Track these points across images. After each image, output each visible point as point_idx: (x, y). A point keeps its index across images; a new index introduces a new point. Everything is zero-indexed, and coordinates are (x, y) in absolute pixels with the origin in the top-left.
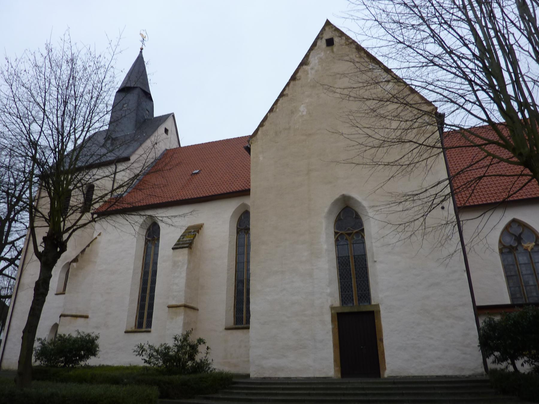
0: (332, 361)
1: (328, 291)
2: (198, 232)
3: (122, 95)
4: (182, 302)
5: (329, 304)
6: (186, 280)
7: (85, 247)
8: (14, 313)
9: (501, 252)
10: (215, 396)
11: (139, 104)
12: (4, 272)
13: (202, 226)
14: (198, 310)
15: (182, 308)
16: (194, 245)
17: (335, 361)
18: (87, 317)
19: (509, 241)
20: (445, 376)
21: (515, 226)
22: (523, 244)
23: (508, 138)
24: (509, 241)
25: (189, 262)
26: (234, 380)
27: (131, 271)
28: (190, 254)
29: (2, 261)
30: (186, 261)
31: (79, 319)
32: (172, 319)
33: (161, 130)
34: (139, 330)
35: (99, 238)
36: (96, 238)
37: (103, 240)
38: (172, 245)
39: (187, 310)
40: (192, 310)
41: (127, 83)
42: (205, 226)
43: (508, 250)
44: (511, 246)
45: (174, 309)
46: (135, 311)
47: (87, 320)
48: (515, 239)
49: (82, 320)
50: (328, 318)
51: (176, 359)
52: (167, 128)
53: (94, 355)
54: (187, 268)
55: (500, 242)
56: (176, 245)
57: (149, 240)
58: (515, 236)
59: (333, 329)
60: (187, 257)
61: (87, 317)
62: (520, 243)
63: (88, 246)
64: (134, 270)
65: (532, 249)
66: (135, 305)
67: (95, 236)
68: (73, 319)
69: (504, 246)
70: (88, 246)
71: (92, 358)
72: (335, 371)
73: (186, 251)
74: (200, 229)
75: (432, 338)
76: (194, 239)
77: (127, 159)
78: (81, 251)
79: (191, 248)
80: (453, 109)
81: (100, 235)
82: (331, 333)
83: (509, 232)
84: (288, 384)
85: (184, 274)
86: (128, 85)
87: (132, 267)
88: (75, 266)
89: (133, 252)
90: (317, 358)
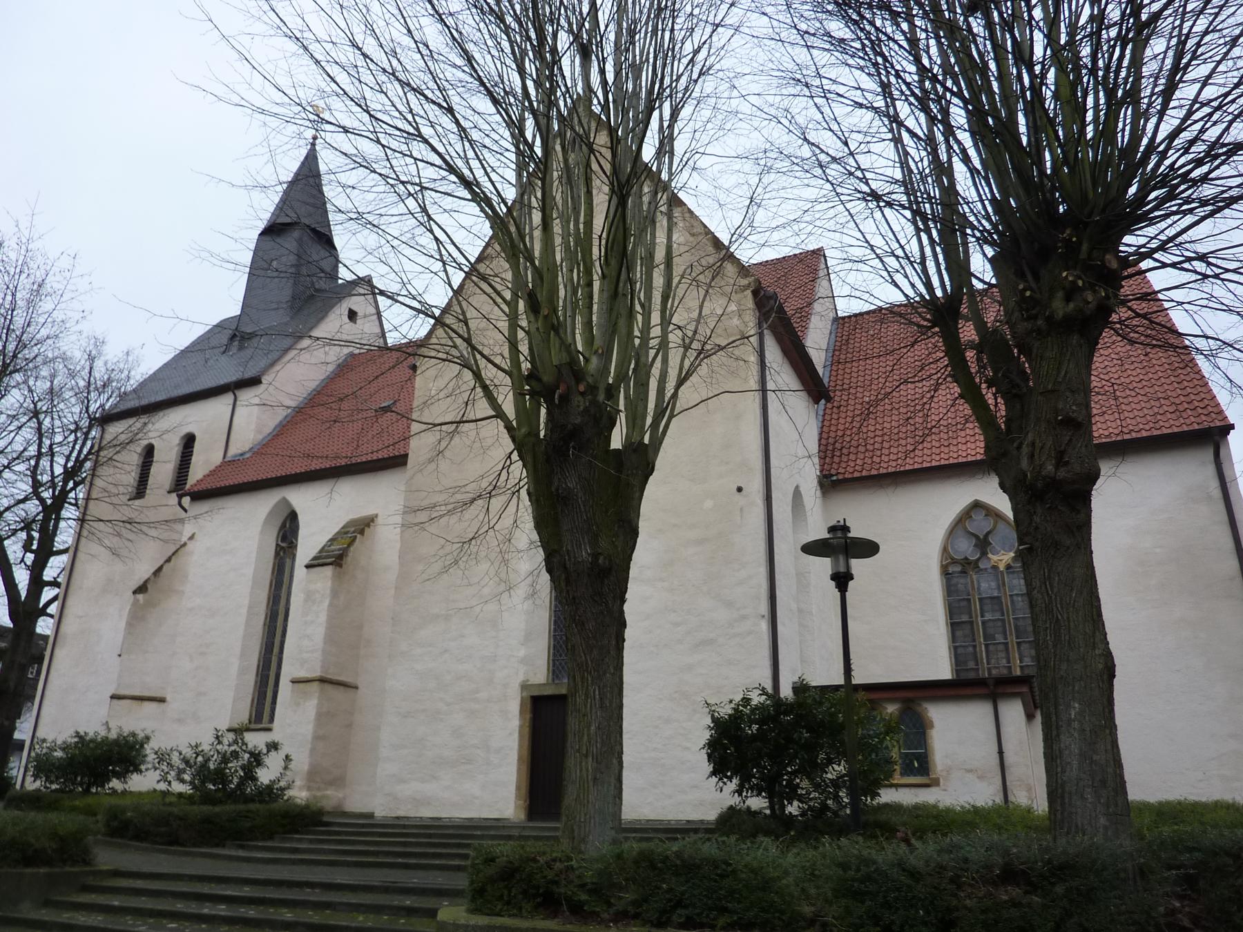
0: (513, 788)
1: (522, 653)
2: (362, 532)
3: (269, 243)
4: (317, 673)
5: (521, 678)
6: (327, 628)
7: (161, 562)
8: (47, 693)
9: (945, 572)
10: (269, 844)
11: (301, 259)
12: (49, 611)
13: (373, 521)
14: (357, 688)
15: (316, 685)
16: (349, 559)
17: (518, 788)
18: (162, 700)
19: (965, 548)
20: (702, 822)
21: (978, 516)
22: (990, 555)
23: (1071, 305)
24: (965, 548)
25: (335, 594)
26: (325, 819)
27: (244, 611)
28: (337, 578)
29: (46, 589)
30: (328, 592)
31: (146, 704)
32: (298, 704)
33: (342, 310)
34: (253, 726)
35: (190, 545)
36: (185, 544)
37: (197, 551)
38: (134, 588)
39: (328, 687)
40: (342, 688)
41: (278, 216)
42: (380, 520)
43: (958, 568)
44: (966, 558)
45: (301, 685)
46: (251, 690)
47: (162, 705)
48: (975, 546)
49: (154, 705)
50: (514, 706)
51: (220, 776)
52: (354, 308)
53: (137, 770)
54: (331, 605)
55: (945, 550)
56: (315, 558)
57: (282, 548)
58: (977, 537)
59: (521, 727)
60: (329, 584)
61: (162, 700)
62: (984, 554)
63: (169, 560)
64: (250, 607)
65: (1008, 567)
66: (251, 678)
67: (184, 539)
68: (135, 703)
69: (952, 559)
70: (169, 560)
71: (135, 777)
72: (516, 807)
73: (328, 571)
74: (368, 525)
75: (687, 749)
76: (350, 544)
77: (254, 381)
78: (152, 570)
79: (341, 566)
80: (498, 360)
81: (191, 538)
82: (516, 735)
83: (965, 529)
84: (404, 826)
85: (323, 618)
86: (280, 221)
87: (246, 602)
88: (141, 601)
89: (249, 571)
90: (483, 782)
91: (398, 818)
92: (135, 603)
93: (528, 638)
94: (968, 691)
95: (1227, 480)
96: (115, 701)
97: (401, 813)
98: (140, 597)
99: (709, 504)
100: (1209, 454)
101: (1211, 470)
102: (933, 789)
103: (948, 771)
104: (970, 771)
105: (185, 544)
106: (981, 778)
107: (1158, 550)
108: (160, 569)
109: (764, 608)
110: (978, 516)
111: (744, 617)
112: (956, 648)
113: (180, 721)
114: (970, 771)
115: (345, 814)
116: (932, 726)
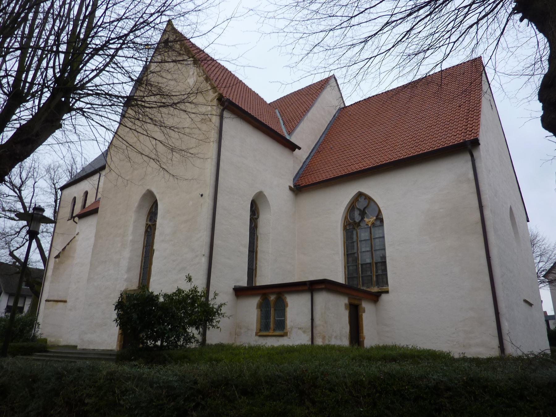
1: (126, 277)
18: (65, 302)
35: (77, 237)
47: (65, 303)
61: (65, 302)
63: (68, 244)
65: (373, 224)
81: (77, 234)
91: (83, 349)
92: (55, 261)
93: (129, 270)
94: (300, 288)
95: (93, 169)
96: (47, 302)
97: (84, 347)
98: (57, 260)
99: (191, 203)
100: (468, 157)
101: (470, 164)
102: (285, 338)
103: (292, 328)
104: (300, 329)
105: (75, 237)
106: (304, 332)
107: (441, 210)
108: (65, 248)
109: (206, 251)
110: (362, 200)
111: (197, 256)
112: (348, 267)
113: (71, 310)
114: (300, 329)
115: (59, 346)
116: (287, 306)
